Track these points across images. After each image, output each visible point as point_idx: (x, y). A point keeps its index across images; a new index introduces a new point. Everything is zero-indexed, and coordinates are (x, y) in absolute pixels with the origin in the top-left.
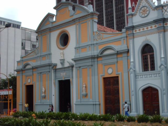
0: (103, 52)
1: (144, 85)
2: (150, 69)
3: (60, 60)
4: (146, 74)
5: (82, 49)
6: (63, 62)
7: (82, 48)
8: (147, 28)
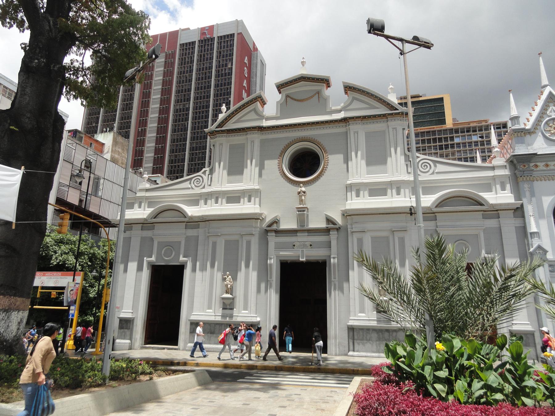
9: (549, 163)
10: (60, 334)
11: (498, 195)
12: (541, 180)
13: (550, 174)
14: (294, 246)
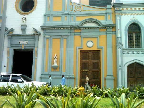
0: (84, 24)
1: (129, 62)
2: (134, 46)
3: (22, 25)
5: (54, 17)
6: (24, 28)
7: (54, 16)
8: (139, 9)
9: (128, 8)
10: (18, 85)
11: (63, 22)
12: (138, 15)
13: (127, 13)
14: (20, 42)
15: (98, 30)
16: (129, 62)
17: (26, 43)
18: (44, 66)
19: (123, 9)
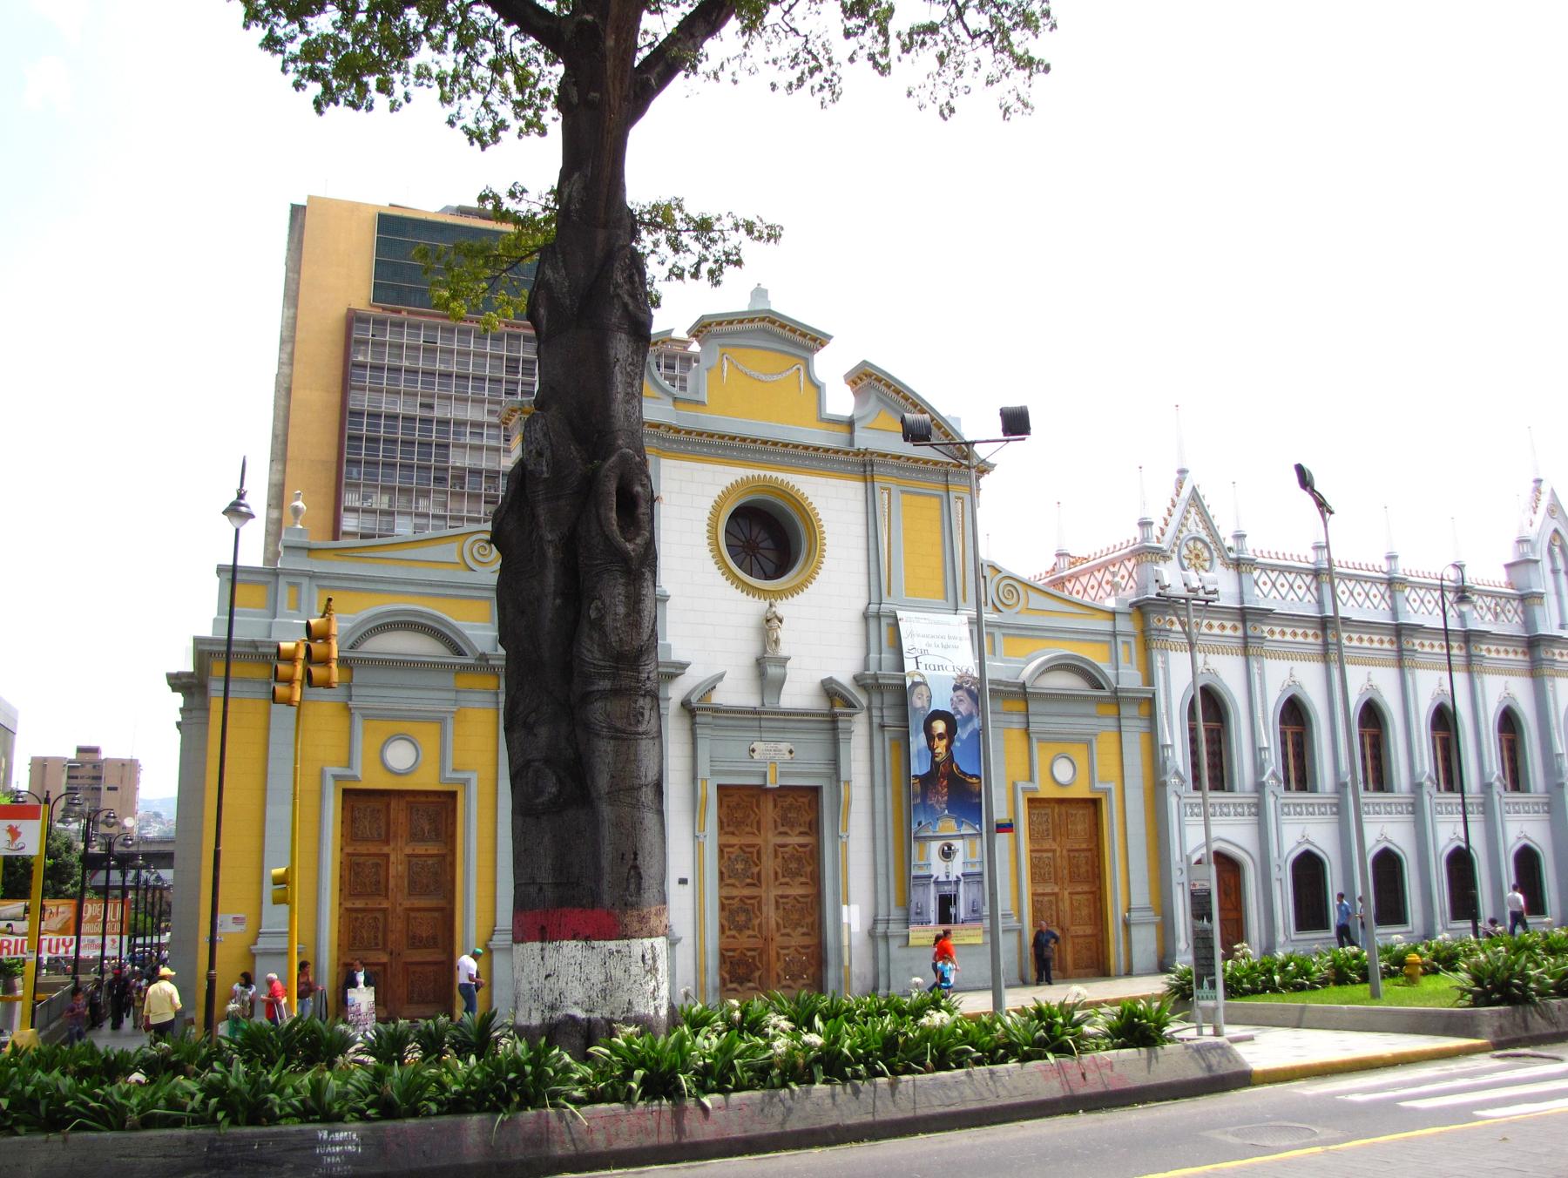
1: (1237, 846)
4: (1370, 800)
11: (276, 620)
14: (753, 751)
15: (449, 680)
16: (1237, 846)
17: (788, 756)
18: (495, 882)
19: (1272, 632)
